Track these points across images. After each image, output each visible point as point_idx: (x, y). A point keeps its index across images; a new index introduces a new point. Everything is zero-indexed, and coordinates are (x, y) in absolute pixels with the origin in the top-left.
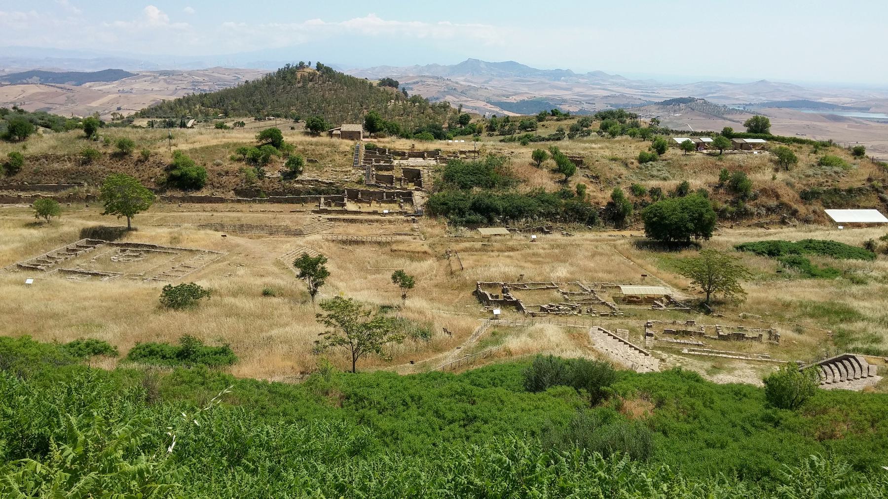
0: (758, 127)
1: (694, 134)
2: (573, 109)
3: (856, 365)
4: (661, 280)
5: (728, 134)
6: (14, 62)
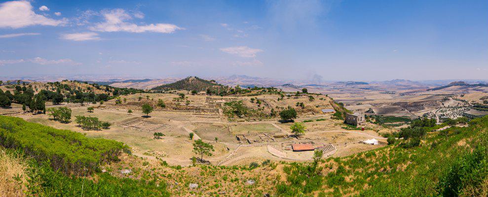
0: (305, 91)
1: (291, 93)
4: (287, 130)
5: (298, 93)
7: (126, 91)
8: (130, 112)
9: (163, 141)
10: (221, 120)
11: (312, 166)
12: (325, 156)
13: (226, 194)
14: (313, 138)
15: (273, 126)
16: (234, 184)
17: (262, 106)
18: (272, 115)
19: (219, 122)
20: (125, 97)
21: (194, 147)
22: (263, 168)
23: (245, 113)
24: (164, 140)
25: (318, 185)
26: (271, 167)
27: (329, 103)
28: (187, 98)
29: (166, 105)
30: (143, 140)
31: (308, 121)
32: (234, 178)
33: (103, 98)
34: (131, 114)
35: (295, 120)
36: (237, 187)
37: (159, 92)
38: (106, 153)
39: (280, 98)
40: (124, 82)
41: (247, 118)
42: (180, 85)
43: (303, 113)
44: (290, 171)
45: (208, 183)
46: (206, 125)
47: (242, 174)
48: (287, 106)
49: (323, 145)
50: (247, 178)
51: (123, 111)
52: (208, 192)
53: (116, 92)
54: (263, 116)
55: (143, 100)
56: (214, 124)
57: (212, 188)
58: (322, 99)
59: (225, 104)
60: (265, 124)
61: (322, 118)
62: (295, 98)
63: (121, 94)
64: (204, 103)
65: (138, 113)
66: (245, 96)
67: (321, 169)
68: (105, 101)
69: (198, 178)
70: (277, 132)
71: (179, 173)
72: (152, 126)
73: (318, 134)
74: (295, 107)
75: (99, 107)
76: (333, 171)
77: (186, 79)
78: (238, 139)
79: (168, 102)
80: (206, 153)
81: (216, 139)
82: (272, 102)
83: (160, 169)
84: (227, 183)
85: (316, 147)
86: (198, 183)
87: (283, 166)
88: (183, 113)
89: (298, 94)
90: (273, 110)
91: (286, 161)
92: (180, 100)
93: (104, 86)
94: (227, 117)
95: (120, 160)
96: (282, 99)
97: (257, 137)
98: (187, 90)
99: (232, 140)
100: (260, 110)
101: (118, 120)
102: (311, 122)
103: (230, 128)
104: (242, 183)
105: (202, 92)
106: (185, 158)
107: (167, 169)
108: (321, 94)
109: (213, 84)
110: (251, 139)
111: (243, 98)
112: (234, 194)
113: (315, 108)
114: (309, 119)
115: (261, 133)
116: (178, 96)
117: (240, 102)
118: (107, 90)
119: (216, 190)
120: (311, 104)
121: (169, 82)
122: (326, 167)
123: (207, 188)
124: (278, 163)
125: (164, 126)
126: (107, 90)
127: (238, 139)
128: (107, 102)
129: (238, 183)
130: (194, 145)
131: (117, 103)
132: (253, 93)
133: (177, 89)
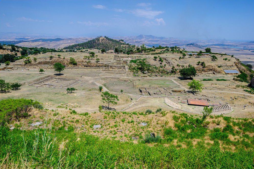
0: (208, 51)
1: (193, 52)
2: (203, 44)
3: (227, 107)
4: (185, 86)
5: (201, 52)
6: (36, 37)
7: (37, 50)
8: (41, 71)
9: (75, 95)
10: (127, 75)
11: (201, 119)
12: (213, 114)
13: (123, 132)
14: (210, 96)
15: (173, 82)
16: (130, 125)
17: (164, 63)
18: (172, 72)
19: (125, 77)
20: (35, 56)
21: (102, 97)
22: (156, 115)
23: (148, 70)
24: (76, 94)
25: (202, 134)
26: (162, 115)
27: (234, 64)
28: (97, 56)
29: (78, 63)
30: (57, 95)
31: (208, 80)
32: (130, 121)
34: (43, 72)
35: (194, 77)
37: (71, 51)
38: (13, 112)
40: (33, 41)
41: (150, 74)
42: (91, 44)
43: (203, 72)
44: (178, 119)
45: (109, 124)
46: (114, 80)
47: (138, 118)
48: (187, 65)
49: (218, 104)
50: (141, 121)
51: (34, 71)
52: (108, 130)
53: (25, 52)
54: (164, 72)
55: (55, 59)
56: (121, 79)
57: (112, 127)
58: (226, 59)
59: (131, 61)
60: (165, 80)
61: (223, 78)
62: (196, 57)
63: (31, 53)
64: (112, 61)
65: (50, 71)
67: (208, 123)
68: (12, 61)
69: (101, 121)
70: (176, 87)
71: (85, 118)
72: (65, 83)
73: (216, 93)
74: (196, 66)
75: (5, 68)
76: (220, 127)
78: (141, 91)
79: (79, 60)
80: (112, 102)
81: (122, 91)
82: (174, 60)
83: (69, 117)
84: (125, 124)
85: (211, 104)
86: (101, 125)
87: (173, 114)
88: (93, 70)
89: (200, 54)
90: (173, 67)
91: (176, 111)
92: (91, 58)
93: (9, 45)
94: (132, 73)
95: (30, 115)
96: (183, 58)
97: (157, 90)
99: (136, 92)
100: (162, 67)
101: (29, 80)
102: (210, 81)
103: (134, 82)
104: (136, 124)
105: (110, 51)
106: (94, 107)
108: (225, 54)
109: (122, 44)
110: (151, 92)
112: (129, 131)
114: (209, 78)
115: (161, 87)
116: (88, 55)
118: (13, 49)
119: (115, 129)
120: (213, 64)
121: (81, 42)
122: (213, 123)
123: (108, 127)
124: (168, 111)
125: (76, 82)
126: (13, 49)
127: (141, 91)
128: (15, 63)
129: (133, 124)
130: (102, 96)
131: (26, 63)
133: (89, 48)
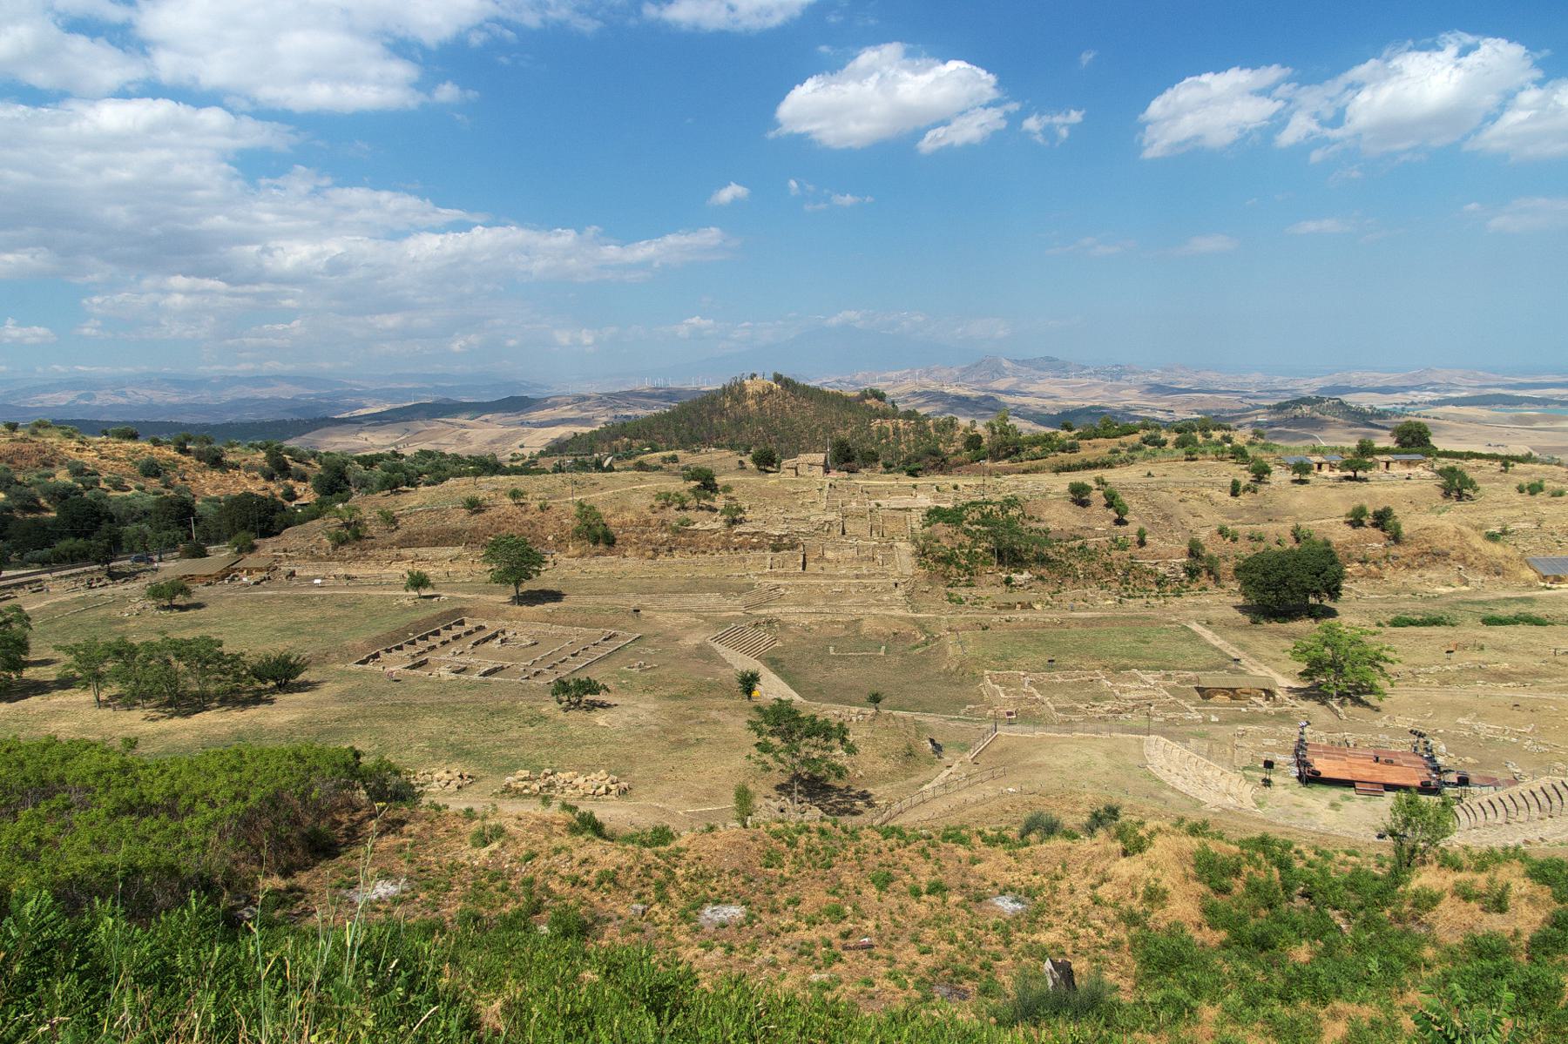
0: (1414, 440)
9: (601, 718)
12: (1465, 835)
28: (727, 489)
31: (1423, 623)
33: (260, 520)
36: (937, 922)
37: (583, 467)
39: (1245, 478)
40: (379, 420)
42: (695, 421)
48: (1284, 528)
57: (812, 923)
58: (1535, 489)
61: (1524, 609)
66: (1037, 470)
77: (726, 391)
79: (629, 516)
83: (557, 851)
86: (747, 903)
98: (732, 447)
107: (596, 848)
108: (1527, 459)
111: (1030, 480)
113: (1477, 542)
117: (1011, 503)
119: (832, 933)
130: (754, 726)
132: (1087, 451)
133: (684, 444)
